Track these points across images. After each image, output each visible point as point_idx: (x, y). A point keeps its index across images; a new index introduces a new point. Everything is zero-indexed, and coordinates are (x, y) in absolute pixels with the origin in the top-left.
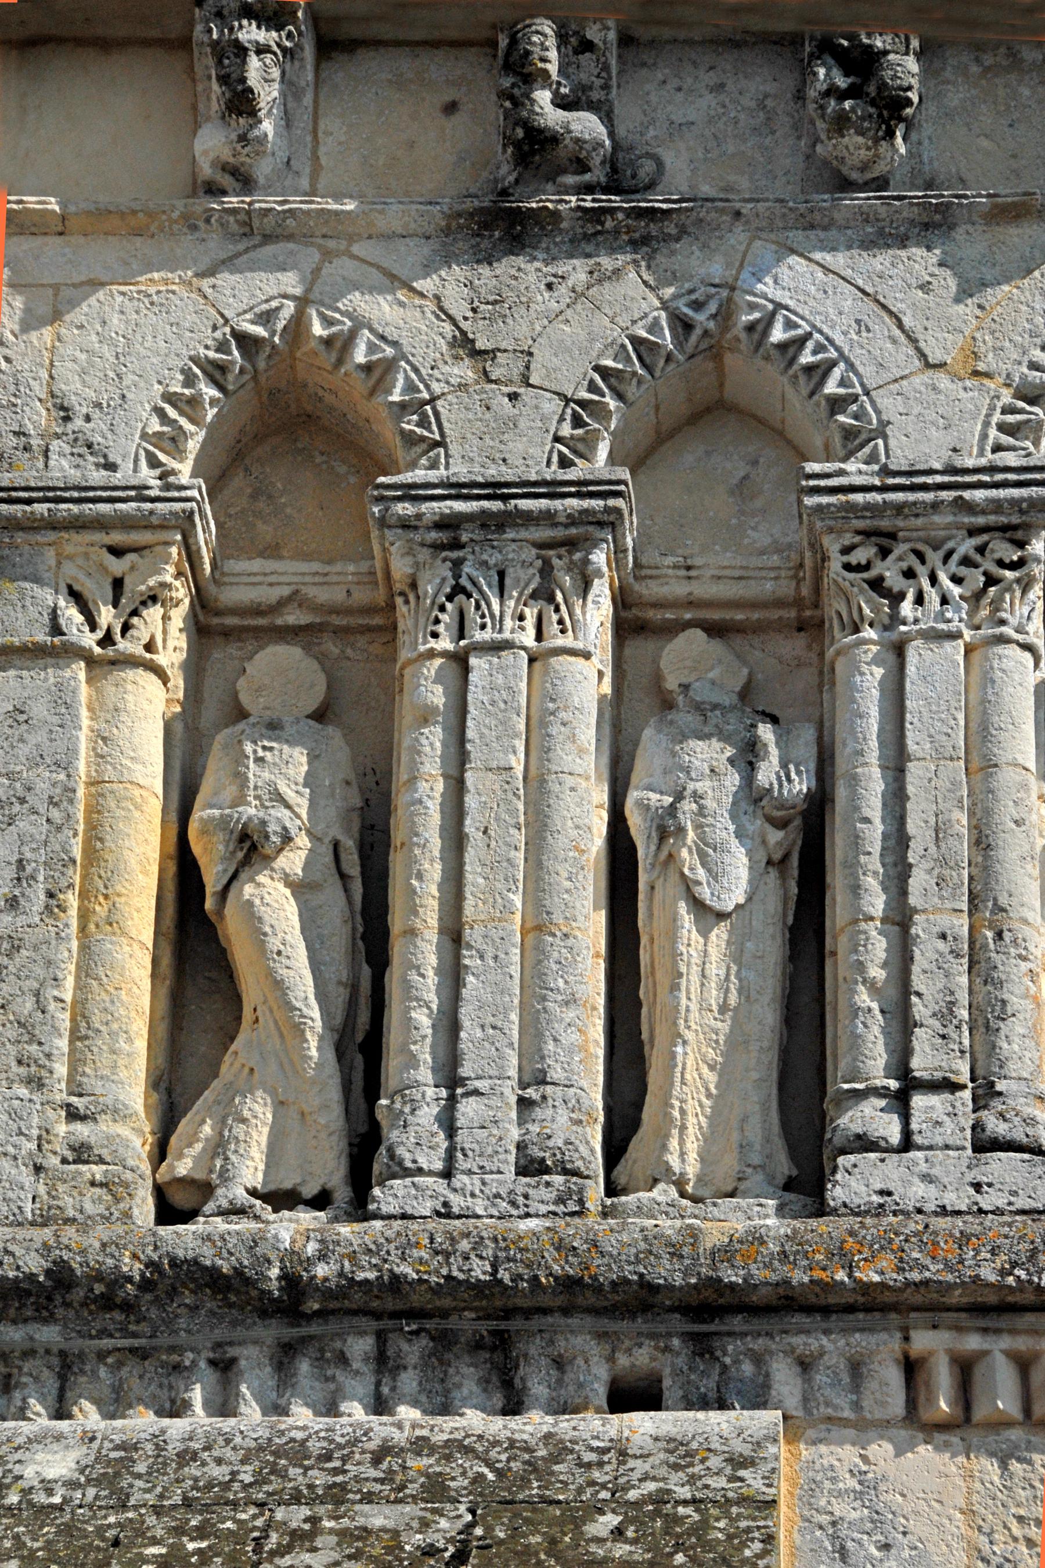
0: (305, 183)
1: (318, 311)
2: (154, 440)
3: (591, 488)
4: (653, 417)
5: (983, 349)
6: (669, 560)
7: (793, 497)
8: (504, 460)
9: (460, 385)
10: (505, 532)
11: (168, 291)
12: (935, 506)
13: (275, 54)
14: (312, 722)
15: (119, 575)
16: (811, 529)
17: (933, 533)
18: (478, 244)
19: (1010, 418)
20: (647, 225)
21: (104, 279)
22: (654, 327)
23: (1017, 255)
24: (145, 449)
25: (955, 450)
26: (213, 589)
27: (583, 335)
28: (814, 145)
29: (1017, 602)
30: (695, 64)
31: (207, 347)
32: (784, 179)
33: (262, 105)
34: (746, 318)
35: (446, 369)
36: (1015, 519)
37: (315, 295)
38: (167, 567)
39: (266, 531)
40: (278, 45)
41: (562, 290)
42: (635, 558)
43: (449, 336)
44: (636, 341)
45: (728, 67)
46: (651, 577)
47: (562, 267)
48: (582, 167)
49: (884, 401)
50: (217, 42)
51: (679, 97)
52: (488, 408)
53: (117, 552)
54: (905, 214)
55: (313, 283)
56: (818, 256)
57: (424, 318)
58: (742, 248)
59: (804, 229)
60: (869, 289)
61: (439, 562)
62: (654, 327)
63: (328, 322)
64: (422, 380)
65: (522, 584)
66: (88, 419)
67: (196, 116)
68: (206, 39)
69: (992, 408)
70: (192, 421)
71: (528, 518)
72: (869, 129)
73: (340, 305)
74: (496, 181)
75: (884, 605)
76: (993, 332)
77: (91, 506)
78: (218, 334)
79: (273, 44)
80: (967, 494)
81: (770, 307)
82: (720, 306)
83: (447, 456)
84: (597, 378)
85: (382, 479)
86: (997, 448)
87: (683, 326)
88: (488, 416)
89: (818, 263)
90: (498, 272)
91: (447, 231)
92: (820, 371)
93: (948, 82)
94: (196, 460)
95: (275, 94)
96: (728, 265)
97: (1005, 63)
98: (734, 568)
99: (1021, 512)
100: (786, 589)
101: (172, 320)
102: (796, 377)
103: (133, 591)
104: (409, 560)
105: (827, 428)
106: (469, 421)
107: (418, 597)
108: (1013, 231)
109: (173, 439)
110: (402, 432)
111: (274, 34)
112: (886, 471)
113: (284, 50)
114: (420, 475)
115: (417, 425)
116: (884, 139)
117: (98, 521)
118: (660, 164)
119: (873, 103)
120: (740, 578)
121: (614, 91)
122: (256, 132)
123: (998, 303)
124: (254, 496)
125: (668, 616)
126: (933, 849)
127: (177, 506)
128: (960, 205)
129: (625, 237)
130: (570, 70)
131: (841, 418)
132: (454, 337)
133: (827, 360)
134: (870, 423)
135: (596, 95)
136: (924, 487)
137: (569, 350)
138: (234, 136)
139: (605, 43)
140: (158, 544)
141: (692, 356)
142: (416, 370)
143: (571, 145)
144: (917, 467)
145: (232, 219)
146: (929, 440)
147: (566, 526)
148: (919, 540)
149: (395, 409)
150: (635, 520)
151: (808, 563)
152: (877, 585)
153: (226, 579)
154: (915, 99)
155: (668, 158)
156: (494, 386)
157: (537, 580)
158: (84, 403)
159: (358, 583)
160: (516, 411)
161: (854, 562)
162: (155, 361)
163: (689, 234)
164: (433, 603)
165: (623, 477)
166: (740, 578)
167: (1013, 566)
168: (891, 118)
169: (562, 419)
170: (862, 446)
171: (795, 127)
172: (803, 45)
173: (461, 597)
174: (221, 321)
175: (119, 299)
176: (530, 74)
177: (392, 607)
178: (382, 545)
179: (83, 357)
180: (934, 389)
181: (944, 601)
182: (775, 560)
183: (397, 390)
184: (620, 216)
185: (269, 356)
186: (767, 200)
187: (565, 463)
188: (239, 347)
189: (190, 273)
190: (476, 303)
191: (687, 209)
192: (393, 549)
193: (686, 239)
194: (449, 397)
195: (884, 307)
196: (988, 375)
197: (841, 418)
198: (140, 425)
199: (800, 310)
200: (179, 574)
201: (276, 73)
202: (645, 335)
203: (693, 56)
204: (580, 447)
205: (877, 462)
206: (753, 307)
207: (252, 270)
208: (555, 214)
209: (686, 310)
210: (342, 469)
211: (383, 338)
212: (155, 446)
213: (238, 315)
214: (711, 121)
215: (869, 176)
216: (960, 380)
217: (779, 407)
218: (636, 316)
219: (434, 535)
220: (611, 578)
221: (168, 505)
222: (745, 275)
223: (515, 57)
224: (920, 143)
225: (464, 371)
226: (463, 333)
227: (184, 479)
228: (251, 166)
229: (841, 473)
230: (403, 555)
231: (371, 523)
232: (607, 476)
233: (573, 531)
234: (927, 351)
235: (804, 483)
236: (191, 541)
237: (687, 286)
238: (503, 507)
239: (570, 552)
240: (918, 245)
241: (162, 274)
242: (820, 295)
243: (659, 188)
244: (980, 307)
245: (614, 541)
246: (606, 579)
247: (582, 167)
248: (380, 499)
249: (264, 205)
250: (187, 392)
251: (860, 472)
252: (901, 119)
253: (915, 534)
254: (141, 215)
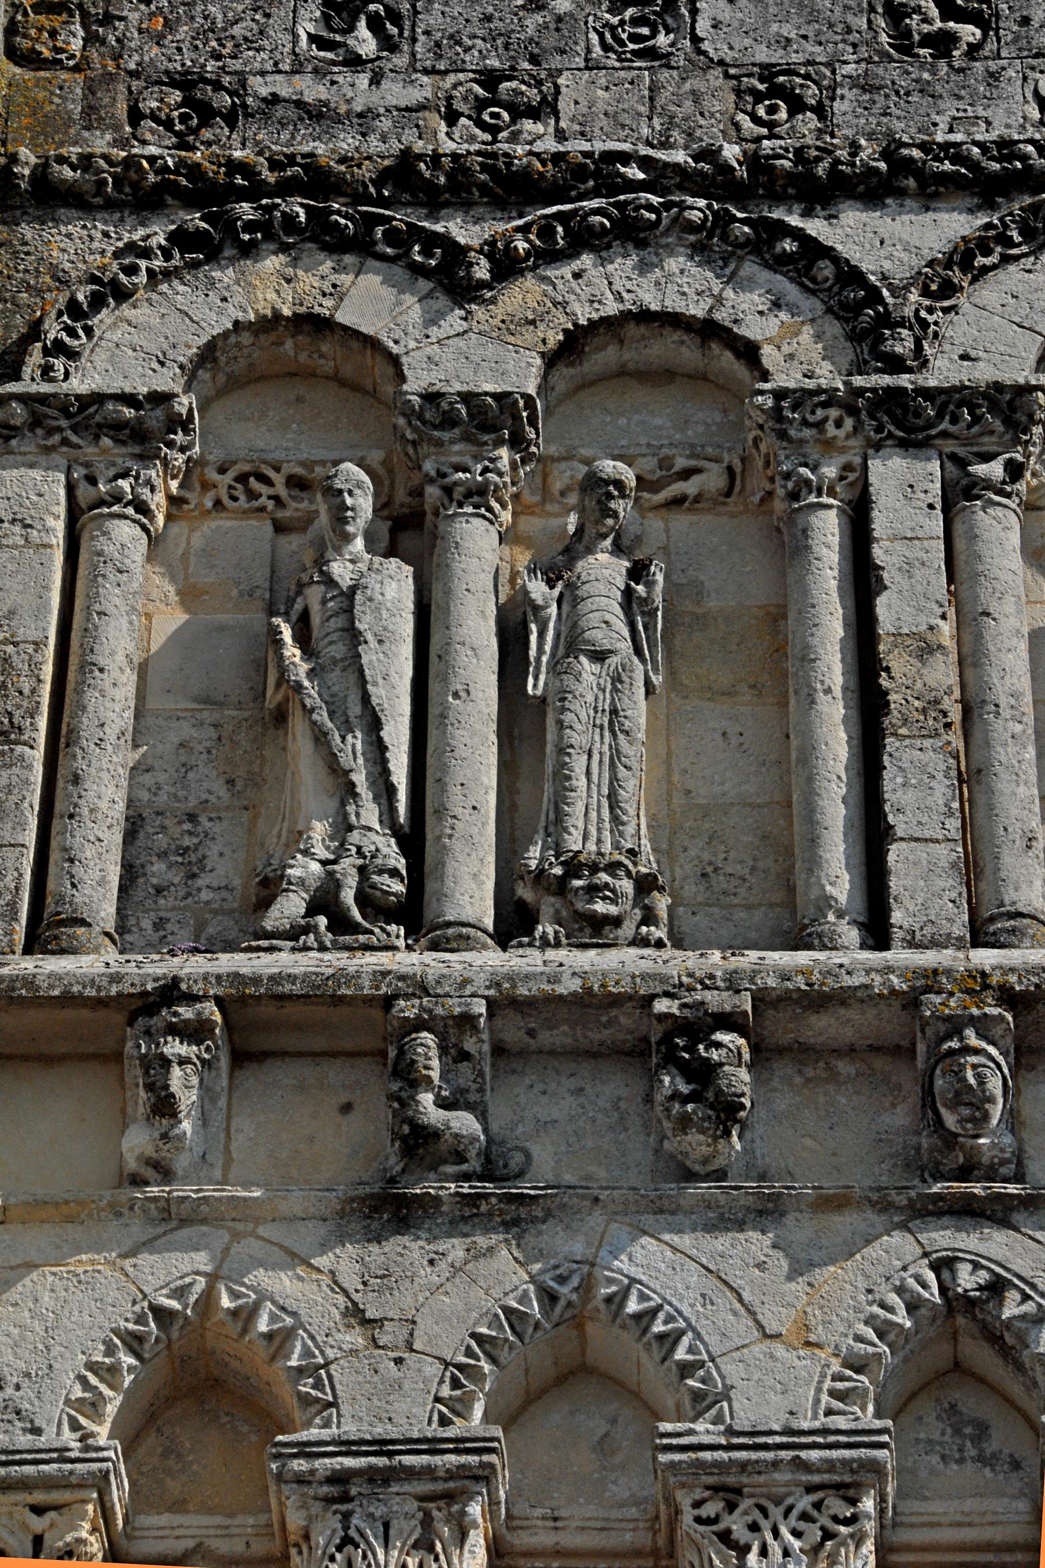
0: (217, 1174)
1: (226, 1285)
2: (76, 1405)
3: (468, 1445)
4: (522, 1378)
5: (813, 1322)
6: (539, 1512)
7: (649, 1453)
8: (390, 1419)
9: (351, 1350)
10: (389, 1486)
11: (94, 1271)
12: (776, 1464)
13: (195, 1064)
15: (39, 1531)
16: (665, 1485)
17: (774, 1489)
18: (369, 1226)
19: (840, 1385)
20: (517, 1209)
21: (38, 1262)
22: (523, 1299)
23: (841, 1239)
24: (68, 1415)
25: (791, 1413)
26: (123, 1543)
27: (461, 1305)
28: (661, 1141)
29: (852, 1556)
30: (557, 1071)
31: (127, 1320)
32: (636, 1171)
33: (182, 1108)
34: (606, 1291)
35: (339, 1336)
36: (847, 1478)
37: (224, 1272)
38: (83, 1524)
39: (174, 1486)
40: (198, 1057)
41: (443, 1265)
42: (507, 1510)
43: (342, 1307)
44: (508, 1311)
45: (586, 1074)
46: (522, 1528)
47: (442, 1246)
48: (460, 1158)
49: (727, 1368)
50: (145, 1056)
51: (544, 1099)
52: (376, 1372)
53: (38, 1510)
54: (742, 1202)
55: (223, 1260)
56: (667, 1237)
57: (320, 1291)
58: (601, 1229)
59: (655, 1213)
60: (712, 1267)
61: (329, 1514)
62: (523, 1299)
63: (235, 1295)
64: (318, 1347)
65: (405, 1535)
66: (18, 1387)
67: (124, 1118)
68: (135, 1054)
69: (823, 1376)
70: (112, 1387)
71: (411, 1473)
72: (708, 1129)
73: (246, 1280)
74: (385, 1170)
75: (732, 1556)
76: (821, 1308)
77: (17, 1468)
78: (137, 1308)
79: (193, 1056)
80: (803, 1454)
81: (626, 1281)
82: (582, 1280)
83: (339, 1415)
85: (280, 1438)
86: (829, 1412)
87: (549, 1298)
88: (376, 1378)
89: (666, 1243)
90: (386, 1250)
91: (342, 1214)
92: (670, 1340)
93: (775, 1090)
94: (113, 1423)
95: (194, 1098)
96: (589, 1244)
97: (824, 1075)
98: (597, 1519)
99: (853, 1471)
100: (643, 1539)
101: (97, 1296)
102: (649, 1343)
103: (51, 1547)
104: (303, 1513)
105: (678, 1391)
106: (359, 1383)
107: (310, 1548)
108: (836, 1219)
109: (93, 1405)
110: (299, 1393)
111: (195, 1048)
112: (730, 1432)
113: (203, 1061)
114: (314, 1433)
115: (313, 1387)
116: (722, 1137)
117: (23, 1483)
118: (528, 1156)
119: (712, 1107)
120: (603, 1529)
121: (488, 1093)
122: (177, 1131)
123: (825, 1282)
124: (165, 1454)
125: (537, 1564)
127: (95, 1466)
128: (790, 1195)
129: (499, 1219)
130: (450, 1076)
131: (690, 1382)
132: (347, 1307)
133: (675, 1330)
134: (716, 1387)
135: (472, 1097)
136: (765, 1447)
137: (448, 1319)
138: (157, 1135)
139: (480, 1053)
140: (76, 1502)
141: (557, 1325)
142: (312, 1338)
143: (451, 1140)
144: (758, 1428)
145: (152, 1206)
146: (768, 1403)
147: (445, 1480)
148: (762, 1495)
149: (293, 1373)
150: (507, 1474)
151: (663, 1517)
152: (725, 1537)
153: (137, 1533)
154: (748, 1104)
155: (535, 1150)
156: (382, 1352)
157: (418, 1532)
158: (15, 1373)
159: (257, 1535)
160: (401, 1374)
161: (704, 1515)
162: (79, 1333)
163: (554, 1217)
164: (324, 1553)
165: (496, 1435)
166: (603, 1529)
167: (847, 1522)
168: (727, 1120)
169: (441, 1381)
170: (709, 1408)
171: (646, 1126)
172: (650, 1056)
173: (350, 1548)
174: (140, 1296)
175: (50, 1278)
176: (416, 1080)
177: (287, 1557)
178: (279, 1499)
179: (16, 1331)
180: (771, 1357)
181: (786, 1553)
182: (633, 1512)
183: (296, 1356)
184: (494, 1200)
185: (182, 1327)
186: (621, 1188)
187: (444, 1421)
188: (156, 1319)
189: (114, 1254)
190: (367, 1278)
191: (551, 1195)
192: (289, 1503)
193: (551, 1222)
194: (342, 1362)
195: (725, 1283)
196: (818, 1345)
197: (690, 1382)
198: (64, 1392)
199: (651, 1285)
200: (94, 1530)
201: (195, 1080)
202: (516, 1305)
203: (556, 1063)
204: (458, 1407)
205: (723, 1422)
206: (610, 1281)
207: (169, 1250)
208: (437, 1199)
209: (552, 1284)
210: (245, 1429)
211: (283, 1309)
212: (77, 1411)
213: (156, 1290)
214: (572, 1119)
215: (710, 1168)
216: (794, 1349)
217: (635, 1371)
218: (508, 1289)
219: (325, 1489)
220: (486, 1529)
221: (86, 1465)
222: (603, 1253)
223: (403, 1065)
224: (753, 1141)
225: (355, 1338)
226: (355, 1304)
227: (102, 1441)
228: (171, 1160)
229: (691, 1432)
230: (297, 1509)
231: (269, 1478)
232: (481, 1434)
233: (452, 1485)
234: (765, 1323)
235: (658, 1441)
236: (106, 1498)
237: (552, 1262)
238: (388, 1463)
239: (449, 1505)
240: (754, 1229)
241: (90, 1256)
242: (670, 1272)
243: (528, 1176)
244: (810, 1284)
245: (489, 1494)
246: (481, 1529)
247: (460, 1158)
248: (277, 1456)
249: (181, 1194)
250: (107, 1360)
251: (708, 1432)
252: (736, 1121)
253: (758, 1490)
254: (73, 1205)
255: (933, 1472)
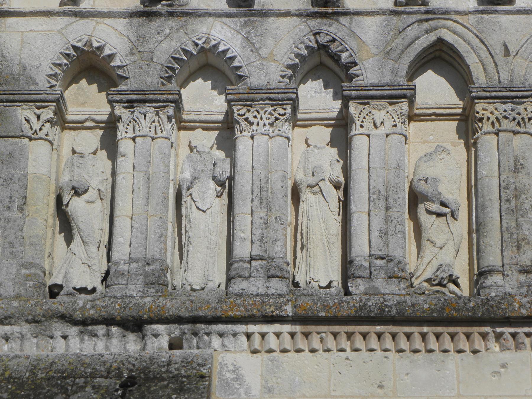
14: (93, 155)
53: (38, 108)
84: (172, 60)
126: (259, 194)
152: (246, 120)
167: (283, 115)
188: (73, 49)
210: (103, 82)
255: (312, 97)
